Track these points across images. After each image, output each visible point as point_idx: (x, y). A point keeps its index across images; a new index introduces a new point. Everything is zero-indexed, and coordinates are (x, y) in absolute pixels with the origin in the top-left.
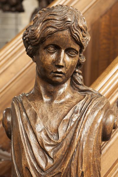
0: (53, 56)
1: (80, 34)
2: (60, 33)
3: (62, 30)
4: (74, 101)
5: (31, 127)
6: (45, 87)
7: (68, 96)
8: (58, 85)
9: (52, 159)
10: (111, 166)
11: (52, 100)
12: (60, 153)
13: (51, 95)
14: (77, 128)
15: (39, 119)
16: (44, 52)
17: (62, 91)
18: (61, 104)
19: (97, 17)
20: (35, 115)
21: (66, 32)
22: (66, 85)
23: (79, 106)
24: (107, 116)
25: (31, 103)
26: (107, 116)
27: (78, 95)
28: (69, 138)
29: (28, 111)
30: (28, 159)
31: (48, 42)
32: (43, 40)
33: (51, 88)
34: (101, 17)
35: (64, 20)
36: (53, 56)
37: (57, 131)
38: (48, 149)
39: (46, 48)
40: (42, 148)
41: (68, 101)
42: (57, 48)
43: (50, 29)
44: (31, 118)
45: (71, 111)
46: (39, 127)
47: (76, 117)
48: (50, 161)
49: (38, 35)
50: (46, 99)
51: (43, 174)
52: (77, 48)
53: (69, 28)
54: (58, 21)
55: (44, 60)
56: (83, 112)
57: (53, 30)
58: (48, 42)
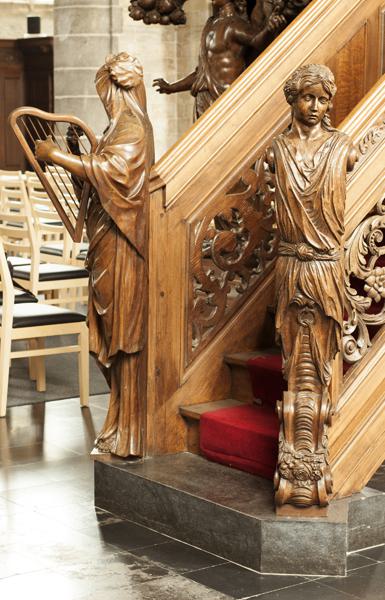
0: (309, 103)
1: (330, 86)
6: (301, 128)
7: (319, 135)
8: (311, 125)
11: (307, 138)
12: (316, 176)
13: (306, 133)
15: (298, 152)
16: (302, 100)
17: (313, 131)
19: (333, 52)
21: (320, 85)
22: (318, 126)
23: (329, 141)
26: (350, 150)
30: (290, 183)
32: (301, 91)
33: (307, 128)
34: (338, 52)
35: (318, 76)
36: (309, 103)
37: (313, 161)
38: (306, 174)
39: (304, 97)
44: (292, 152)
46: (298, 157)
47: (327, 150)
48: (307, 184)
49: (298, 88)
50: (303, 137)
52: (327, 97)
53: (322, 82)
54: (312, 78)
56: (332, 147)
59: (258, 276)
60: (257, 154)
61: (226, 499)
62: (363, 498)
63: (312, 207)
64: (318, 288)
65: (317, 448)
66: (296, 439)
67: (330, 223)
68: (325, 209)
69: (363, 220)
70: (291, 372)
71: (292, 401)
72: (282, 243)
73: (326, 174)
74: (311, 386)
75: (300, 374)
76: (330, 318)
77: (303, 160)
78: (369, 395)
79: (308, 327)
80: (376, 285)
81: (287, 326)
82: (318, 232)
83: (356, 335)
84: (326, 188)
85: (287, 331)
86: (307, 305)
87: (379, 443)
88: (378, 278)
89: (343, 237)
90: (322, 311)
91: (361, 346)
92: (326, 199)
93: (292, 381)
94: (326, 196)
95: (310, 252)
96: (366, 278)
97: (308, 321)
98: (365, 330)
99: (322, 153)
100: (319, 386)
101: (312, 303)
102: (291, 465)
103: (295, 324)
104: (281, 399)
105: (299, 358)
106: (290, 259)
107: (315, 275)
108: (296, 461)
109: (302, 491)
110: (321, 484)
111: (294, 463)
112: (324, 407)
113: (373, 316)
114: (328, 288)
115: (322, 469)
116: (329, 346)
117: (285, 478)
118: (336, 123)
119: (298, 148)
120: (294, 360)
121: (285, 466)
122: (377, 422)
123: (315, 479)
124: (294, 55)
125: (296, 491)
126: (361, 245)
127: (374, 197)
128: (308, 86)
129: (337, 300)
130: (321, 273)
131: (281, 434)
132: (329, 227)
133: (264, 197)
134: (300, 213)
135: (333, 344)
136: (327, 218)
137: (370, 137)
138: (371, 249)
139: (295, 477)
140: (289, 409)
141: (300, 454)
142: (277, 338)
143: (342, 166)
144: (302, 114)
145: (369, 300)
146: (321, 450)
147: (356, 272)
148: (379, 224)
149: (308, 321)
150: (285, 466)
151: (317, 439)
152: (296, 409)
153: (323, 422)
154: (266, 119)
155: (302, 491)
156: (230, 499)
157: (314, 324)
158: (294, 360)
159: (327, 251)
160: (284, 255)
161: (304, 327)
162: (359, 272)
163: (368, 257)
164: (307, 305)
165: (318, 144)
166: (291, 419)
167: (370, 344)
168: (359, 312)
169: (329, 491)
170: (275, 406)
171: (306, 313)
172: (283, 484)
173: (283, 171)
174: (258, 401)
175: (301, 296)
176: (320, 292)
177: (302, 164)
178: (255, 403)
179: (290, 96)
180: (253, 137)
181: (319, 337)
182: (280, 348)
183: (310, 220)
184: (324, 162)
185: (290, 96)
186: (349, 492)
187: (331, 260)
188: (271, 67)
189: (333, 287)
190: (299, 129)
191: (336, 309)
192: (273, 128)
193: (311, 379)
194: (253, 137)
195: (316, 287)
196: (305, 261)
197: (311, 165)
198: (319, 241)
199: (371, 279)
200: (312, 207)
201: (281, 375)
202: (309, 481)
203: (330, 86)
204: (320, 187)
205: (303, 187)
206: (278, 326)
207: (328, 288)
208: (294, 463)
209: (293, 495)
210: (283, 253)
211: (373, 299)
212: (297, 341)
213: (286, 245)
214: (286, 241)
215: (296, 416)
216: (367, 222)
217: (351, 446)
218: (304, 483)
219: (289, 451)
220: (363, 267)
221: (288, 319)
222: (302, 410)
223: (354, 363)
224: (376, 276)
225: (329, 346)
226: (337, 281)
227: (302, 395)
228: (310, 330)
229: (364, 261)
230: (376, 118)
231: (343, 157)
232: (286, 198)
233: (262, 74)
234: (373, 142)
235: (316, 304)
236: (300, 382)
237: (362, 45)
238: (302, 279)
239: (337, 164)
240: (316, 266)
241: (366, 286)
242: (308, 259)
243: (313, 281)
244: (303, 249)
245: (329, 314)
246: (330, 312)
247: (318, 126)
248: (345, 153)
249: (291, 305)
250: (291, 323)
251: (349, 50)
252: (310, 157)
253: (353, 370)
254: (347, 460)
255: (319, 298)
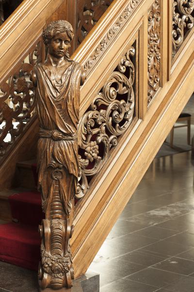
0: (59, 44)
1: (71, 34)
2: (62, 33)
3: (63, 32)
4: (67, 66)
5: (48, 78)
6: (53, 59)
7: (63, 64)
8: (59, 58)
9: (59, 93)
10: (115, 53)
11: (57, 65)
12: (63, 90)
13: (56, 63)
14: (70, 78)
15: (52, 74)
16: (54, 42)
17: (60, 62)
18: (61, 67)
19: (50, 14)
20: (50, 73)
21: (65, 33)
22: (63, 58)
23: (70, 67)
24: (82, 73)
25: (47, 67)
26: (82, 73)
27: (68, 63)
28: (67, 82)
29: (46, 71)
30: (48, 93)
31: (56, 38)
32: (54, 36)
33: (56, 59)
34: (52, 14)
35: (64, 27)
36: (59, 44)
37: (61, 80)
38: (57, 88)
39: (56, 40)
40: (54, 88)
41: (64, 66)
42: (61, 41)
43: (58, 32)
44: (48, 74)
45: (67, 70)
46: (52, 77)
47: (69, 73)
48: (58, 94)
49: (52, 34)
50: (54, 65)
51: (55, 99)
52: (69, 40)
53: (67, 31)
54: (61, 29)
55: (55, 46)
56: (72, 71)
57: (59, 32)
58: (56, 38)
59: (11, 146)
60: (9, 74)
61: (7, 285)
62: (88, 279)
63: (61, 108)
64: (65, 157)
65: (65, 253)
66: (52, 248)
67: (70, 118)
68: (69, 109)
69: (84, 114)
70: (48, 208)
71: (49, 225)
72: (42, 130)
73: (69, 87)
74: (60, 216)
75: (53, 208)
76: (72, 174)
77: (55, 79)
78: (89, 217)
79: (58, 180)
80: (91, 152)
81: (45, 180)
82: (65, 123)
83: (81, 182)
84: (69, 96)
85: (45, 183)
86: (58, 167)
87: (94, 245)
88: (92, 148)
89: (78, 125)
90: (67, 170)
91: (84, 188)
92: (69, 103)
93: (48, 213)
94: (70, 101)
95: (60, 136)
96: (86, 148)
97: (58, 177)
98: (86, 179)
99: (66, 74)
100: (65, 215)
101: (61, 166)
102: (50, 265)
103: (50, 178)
104: (43, 225)
105: (52, 199)
106: (47, 139)
107: (63, 149)
108: (53, 262)
109: (57, 280)
110: (68, 275)
111: (52, 263)
112: (69, 228)
113: (89, 170)
114: (71, 157)
115: (69, 266)
116: (70, 191)
117: (47, 273)
118: (71, 54)
119: (51, 71)
120: (50, 200)
121: (47, 266)
122: (94, 232)
123: (65, 272)
124: (29, 16)
125: (54, 280)
126: (83, 128)
127: (89, 101)
128: (58, 33)
129: (75, 164)
130: (67, 148)
131: (42, 246)
132: (71, 120)
133: (10, 96)
134: (54, 112)
135: (73, 191)
136: (70, 114)
137: (88, 63)
138: (88, 131)
139: (53, 271)
140: (48, 230)
141: (55, 257)
142: (38, 188)
143: (78, 82)
144: (54, 51)
145: (87, 161)
146: (67, 254)
147: (80, 145)
148: (93, 116)
149: (58, 177)
150: (47, 266)
151: (65, 248)
152: (51, 230)
153: (67, 237)
154: (15, 53)
155: (57, 280)
156: (9, 285)
157: (62, 178)
158: (50, 200)
159: (70, 134)
160: (43, 137)
161: (56, 180)
162: (82, 145)
163: (86, 136)
164: (58, 167)
165: (63, 69)
166: (49, 236)
167: (89, 187)
168: (82, 169)
169: (72, 278)
170: (38, 229)
171: (57, 172)
172: (46, 276)
173: (43, 86)
174: (16, 220)
175: (54, 162)
176: (66, 160)
177: (55, 81)
178: (13, 221)
179: (47, 40)
180: (7, 63)
181: (65, 186)
182: (40, 193)
183: (60, 115)
184: (68, 80)
185: (47, 40)
186: (79, 275)
187: (72, 140)
188: (17, 22)
189: (74, 156)
190: (51, 60)
191: (75, 170)
192: (18, 58)
193: (60, 211)
194: (7, 63)
195: (64, 156)
196: (57, 140)
197: (60, 82)
198: (66, 129)
199: (88, 149)
200: (61, 108)
201: (41, 210)
202: (61, 274)
203: (71, 34)
204: (66, 95)
205: (55, 96)
206: (40, 181)
207: (71, 157)
208: (52, 263)
209: (52, 282)
210: (42, 136)
211: (89, 160)
212: (52, 189)
213: (45, 131)
214: (44, 128)
215: (52, 233)
216: (86, 115)
217: (81, 248)
218: (58, 275)
219: (49, 256)
220: (84, 142)
221: (46, 176)
222: (56, 231)
223: (80, 198)
224: (91, 146)
225: (70, 191)
226: (76, 152)
227: (55, 221)
228: (59, 182)
229: (85, 138)
230: (91, 53)
231: (79, 77)
232: (45, 103)
233: (12, 27)
234: (89, 67)
235: (64, 167)
236: (54, 213)
237: (65, 10)
238: (55, 151)
239: (75, 81)
240: (64, 143)
241: (85, 153)
242: (59, 139)
243: (62, 153)
244: (56, 133)
245: (72, 172)
246: (72, 171)
247: (63, 58)
248: (79, 75)
249: (48, 168)
250: (47, 178)
251: (58, 13)
252: (59, 77)
253: (81, 203)
254: (78, 256)
255: (66, 163)
